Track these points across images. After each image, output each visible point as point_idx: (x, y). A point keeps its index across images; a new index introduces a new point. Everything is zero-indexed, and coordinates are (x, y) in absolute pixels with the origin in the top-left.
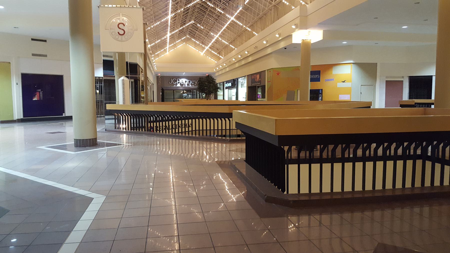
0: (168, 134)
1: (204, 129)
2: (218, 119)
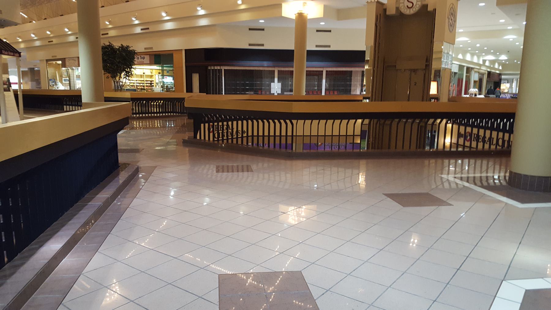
0: (208, 142)
1: (260, 135)
2: (270, 120)
